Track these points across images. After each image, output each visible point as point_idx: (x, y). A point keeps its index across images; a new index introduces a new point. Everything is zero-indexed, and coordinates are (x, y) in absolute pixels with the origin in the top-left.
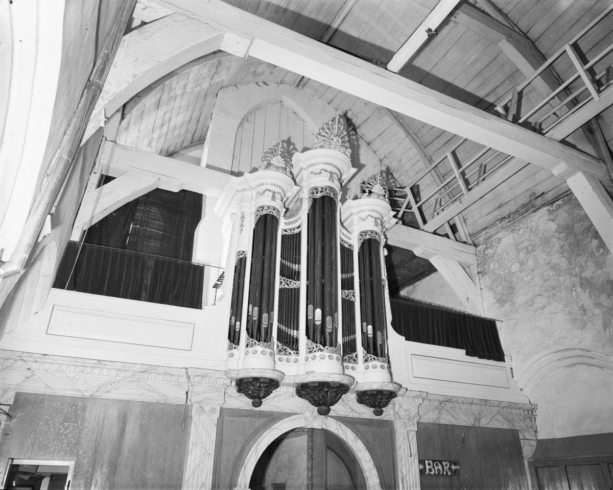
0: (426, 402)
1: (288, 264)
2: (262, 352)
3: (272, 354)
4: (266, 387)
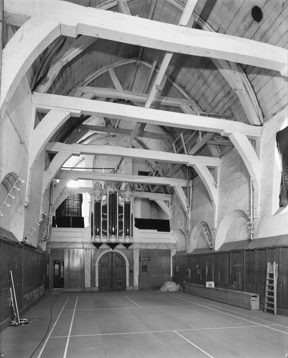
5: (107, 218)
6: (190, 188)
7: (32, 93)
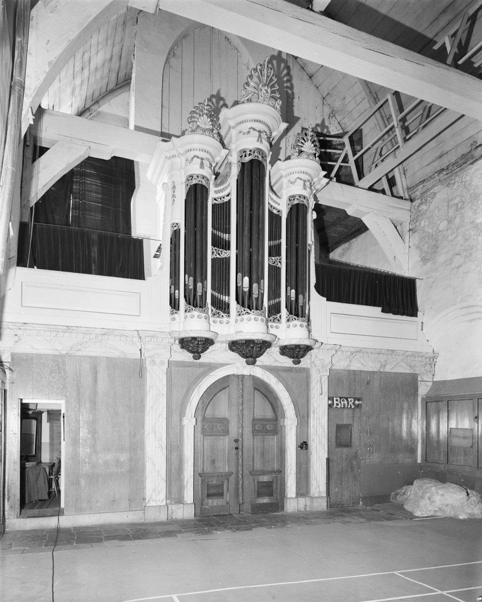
0: (339, 353)
1: (219, 234)
2: (198, 317)
3: (207, 318)
4: (203, 344)
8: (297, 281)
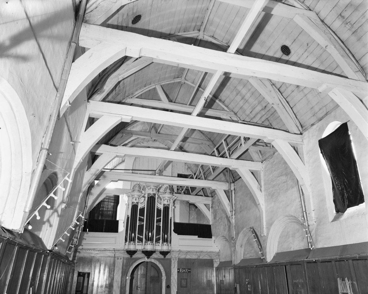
5: (143, 221)
6: (231, 191)
7: (88, 101)
8: (166, 231)
